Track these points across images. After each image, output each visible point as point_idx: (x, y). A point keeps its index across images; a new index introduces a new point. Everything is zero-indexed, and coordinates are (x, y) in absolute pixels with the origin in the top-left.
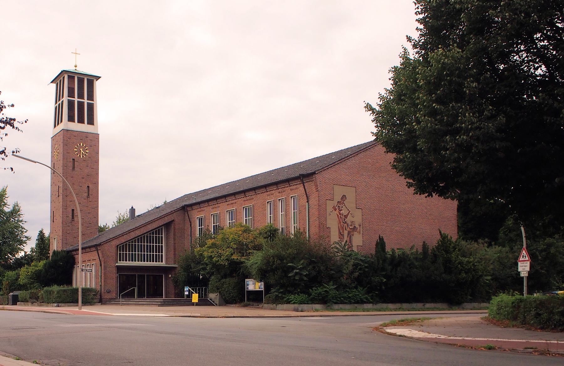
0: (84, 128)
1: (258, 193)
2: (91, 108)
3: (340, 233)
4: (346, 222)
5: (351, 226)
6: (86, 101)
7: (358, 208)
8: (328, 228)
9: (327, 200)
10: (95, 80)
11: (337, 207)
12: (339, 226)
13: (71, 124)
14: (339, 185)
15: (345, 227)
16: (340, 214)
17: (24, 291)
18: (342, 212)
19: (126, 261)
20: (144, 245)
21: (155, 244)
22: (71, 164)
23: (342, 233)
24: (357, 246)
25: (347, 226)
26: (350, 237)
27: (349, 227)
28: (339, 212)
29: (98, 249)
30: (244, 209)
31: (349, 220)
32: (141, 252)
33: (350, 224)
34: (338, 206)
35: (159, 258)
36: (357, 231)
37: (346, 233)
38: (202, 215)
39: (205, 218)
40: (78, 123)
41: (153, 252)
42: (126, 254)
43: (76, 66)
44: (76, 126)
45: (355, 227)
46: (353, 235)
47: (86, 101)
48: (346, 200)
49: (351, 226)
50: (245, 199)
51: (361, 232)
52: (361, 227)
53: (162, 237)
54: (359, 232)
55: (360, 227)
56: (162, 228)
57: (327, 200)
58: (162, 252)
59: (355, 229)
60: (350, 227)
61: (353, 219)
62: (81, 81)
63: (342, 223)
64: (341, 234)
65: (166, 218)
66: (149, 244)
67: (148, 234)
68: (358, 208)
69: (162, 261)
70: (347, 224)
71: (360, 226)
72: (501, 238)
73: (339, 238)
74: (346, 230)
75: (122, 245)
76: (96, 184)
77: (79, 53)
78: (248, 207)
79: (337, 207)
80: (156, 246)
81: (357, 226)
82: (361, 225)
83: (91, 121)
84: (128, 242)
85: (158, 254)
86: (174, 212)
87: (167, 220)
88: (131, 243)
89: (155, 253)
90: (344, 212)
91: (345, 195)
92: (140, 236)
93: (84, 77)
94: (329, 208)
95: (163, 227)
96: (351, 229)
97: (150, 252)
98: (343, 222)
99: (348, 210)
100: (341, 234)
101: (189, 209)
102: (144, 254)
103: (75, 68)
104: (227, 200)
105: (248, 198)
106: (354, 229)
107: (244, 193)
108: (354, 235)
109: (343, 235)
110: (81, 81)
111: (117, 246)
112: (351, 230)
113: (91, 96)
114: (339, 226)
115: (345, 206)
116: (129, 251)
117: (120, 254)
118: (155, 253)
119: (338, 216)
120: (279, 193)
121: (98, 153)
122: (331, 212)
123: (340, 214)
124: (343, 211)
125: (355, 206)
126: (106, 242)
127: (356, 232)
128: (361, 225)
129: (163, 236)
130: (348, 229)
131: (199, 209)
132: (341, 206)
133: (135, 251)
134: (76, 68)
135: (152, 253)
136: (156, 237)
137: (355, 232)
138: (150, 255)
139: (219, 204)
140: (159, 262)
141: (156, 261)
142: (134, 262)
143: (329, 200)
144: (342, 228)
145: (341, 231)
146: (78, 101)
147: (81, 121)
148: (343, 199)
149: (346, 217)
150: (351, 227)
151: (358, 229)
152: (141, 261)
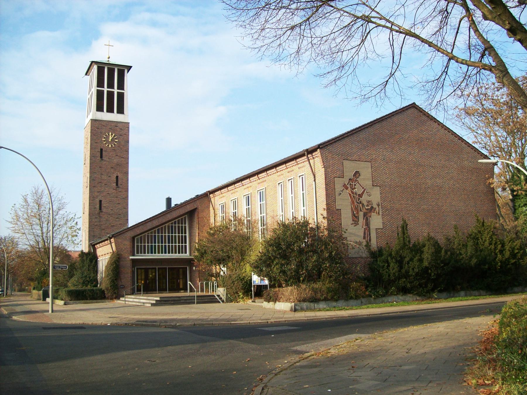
0: (114, 117)
1: (270, 174)
2: (121, 97)
3: (353, 215)
4: (361, 202)
5: (367, 206)
6: (116, 91)
7: (375, 186)
8: (338, 210)
9: (335, 177)
10: (126, 71)
11: (349, 186)
12: (352, 207)
13: (99, 113)
14: (351, 160)
15: (360, 207)
16: (353, 193)
17: (37, 291)
18: (355, 190)
19: (145, 253)
20: (165, 236)
21: (177, 235)
22: (99, 154)
23: (356, 215)
24: (376, 229)
25: (363, 207)
26: (367, 218)
27: (365, 208)
28: (351, 190)
29: (112, 242)
30: (258, 192)
31: (364, 199)
32: (162, 243)
33: (365, 204)
34: (350, 184)
35: (182, 250)
36: (375, 211)
37: (361, 214)
38: (223, 201)
39: (225, 204)
40: (97, 112)
41: (175, 243)
42: (145, 246)
43: (109, 58)
44: (105, 116)
45: (372, 207)
46: (370, 216)
47: (106, 89)
48: (360, 177)
49: (367, 206)
50: (259, 181)
51: (380, 213)
52: (380, 207)
53: (185, 227)
54: (377, 213)
55: (379, 207)
56: (186, 217)
57: (335, 177)
58: (186, 243)
59: (372, 209)
60: (366, 207)
61: (369, 199)
62: (111, 72)
63: (356, 203)
64: (356, 217)
65: (187, 206)
66: (170, 235)
67: (169, 224)
68: (375, 186)
69: (186, 253)
70: (363, 205)
71: (378, 205)
72: (478, 382)
73: (353, 220)
74: (361, 211)
75: (144, 234)
76: (127, 173)
77: (112, 45)
78: (262, 190)
79: (349, 186)
80: (179, 236)
81: (375, 206)
82: (380, 204)
83: (121, 110)
84: (146, 233)
85: (181, 244)
86: (197, 199)
87: (189, 208)
88: (150, 234)
89: (177, 244)
90: (358, 190)
91: (358, 171)
92: (154, 228)
93: (104, 66)
94: (339, 187)
95: (186, 216)
96: (368, 210)
97: (162, 243)
98: (357, 203)
99: (363, 188)
100: (356, 217)
101: (211, 195)
102: (165, 246)
103: (107, 60)
104: (243, 184)
105: (261, 180)
106: (371, 210)
107: (258, 176)
108: (372, 216)
109: (357, 218)
110: (111, 72)
111: (133, 238)
112: (367, 211)
113: (121, 86)
114: (352, 207)
115: (359, 183)
116: (148, 243)
117: (138, 246)
118: (177, 244)
119: (350, 194)
120: (289, 172)
121: (128, 142)
122: (341, 191)
123: (353, 193)
124: (356, 190)
125: (372, 183)
126: (119, 234)
127: (374, 213)
128: (380, 204)
129: (187, 225)
130: (364, 210)
131: (221, 195)
132: (354, 184)
133: (155, 243)
134: (109, 59)
135: (174, 244)
136: (179, 227)
137: (373, 212)
138: (162, 246)
139: (237, 189)
140: (182, 253)
141: (179, 253)
142: (153, 254)
143: (338, 177)
144: (356, 209)
145: (355, 213)
146: (97, 90)
147: (110, 110)
148: (355, 175)
149: (361, 196)
150: (367, 208)
151: (377, 210)
152: (172, 253)
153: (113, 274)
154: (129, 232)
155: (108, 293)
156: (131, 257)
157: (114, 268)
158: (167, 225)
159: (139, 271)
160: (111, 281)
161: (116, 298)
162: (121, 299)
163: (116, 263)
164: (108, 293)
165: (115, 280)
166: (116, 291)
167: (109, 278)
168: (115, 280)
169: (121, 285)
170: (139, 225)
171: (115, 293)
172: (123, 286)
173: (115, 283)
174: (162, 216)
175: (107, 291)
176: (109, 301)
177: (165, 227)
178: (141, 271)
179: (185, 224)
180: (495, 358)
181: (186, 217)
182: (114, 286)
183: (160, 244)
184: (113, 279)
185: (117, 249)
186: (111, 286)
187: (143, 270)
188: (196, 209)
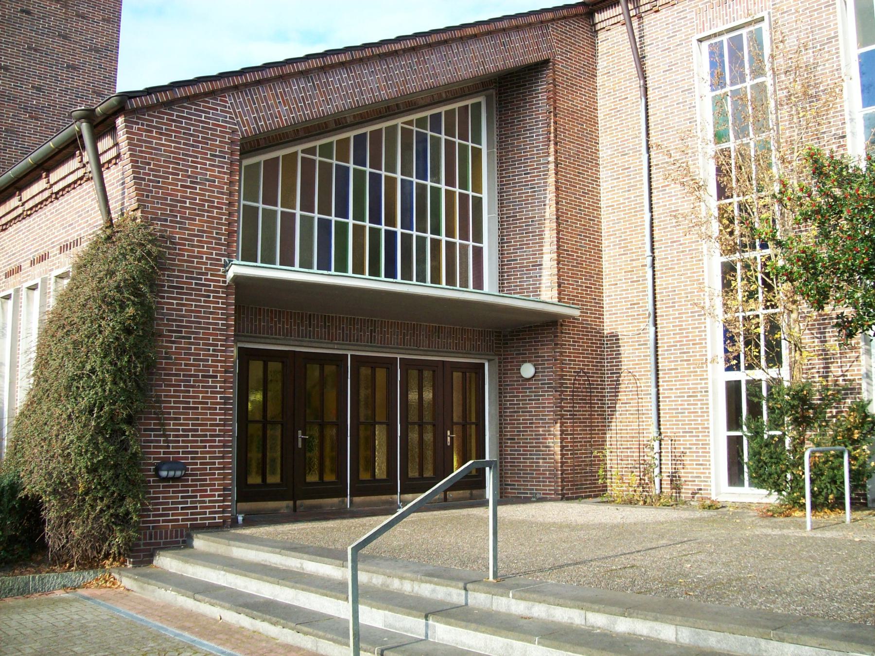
56: (479, 104)
129: (484, 147)
153: (117, 374)
154: (229, 100)
155: (69, 517)
156: (238, 269)
157: (128, 331)
158: (399, 122)
159: (365, 371)
160: (99, 430)
161: (121, 557)
162: (166, 562)
163: (137, 293)
164: (69, 517)
165: (129, 420)
166: (129, 504)
167: (83, 403)
168: (129, 420)
169: (164, 463)
170: (288, 69)
171: (124, 520)
172: (175, 464)
173: (124, 446)
174: (405, 51)
175: (63, 506)
176: (74, 576)
177: (291, 159)
178: (322, 370)
179: (477, 139)
180: (115, 368)
181: (479, 104)
182: (116, 466)
183: (367, 224)
184: (112, 416)
185: (141, 205)
186: (92, 470)
187: (275, 366)
188: (543, 65)
